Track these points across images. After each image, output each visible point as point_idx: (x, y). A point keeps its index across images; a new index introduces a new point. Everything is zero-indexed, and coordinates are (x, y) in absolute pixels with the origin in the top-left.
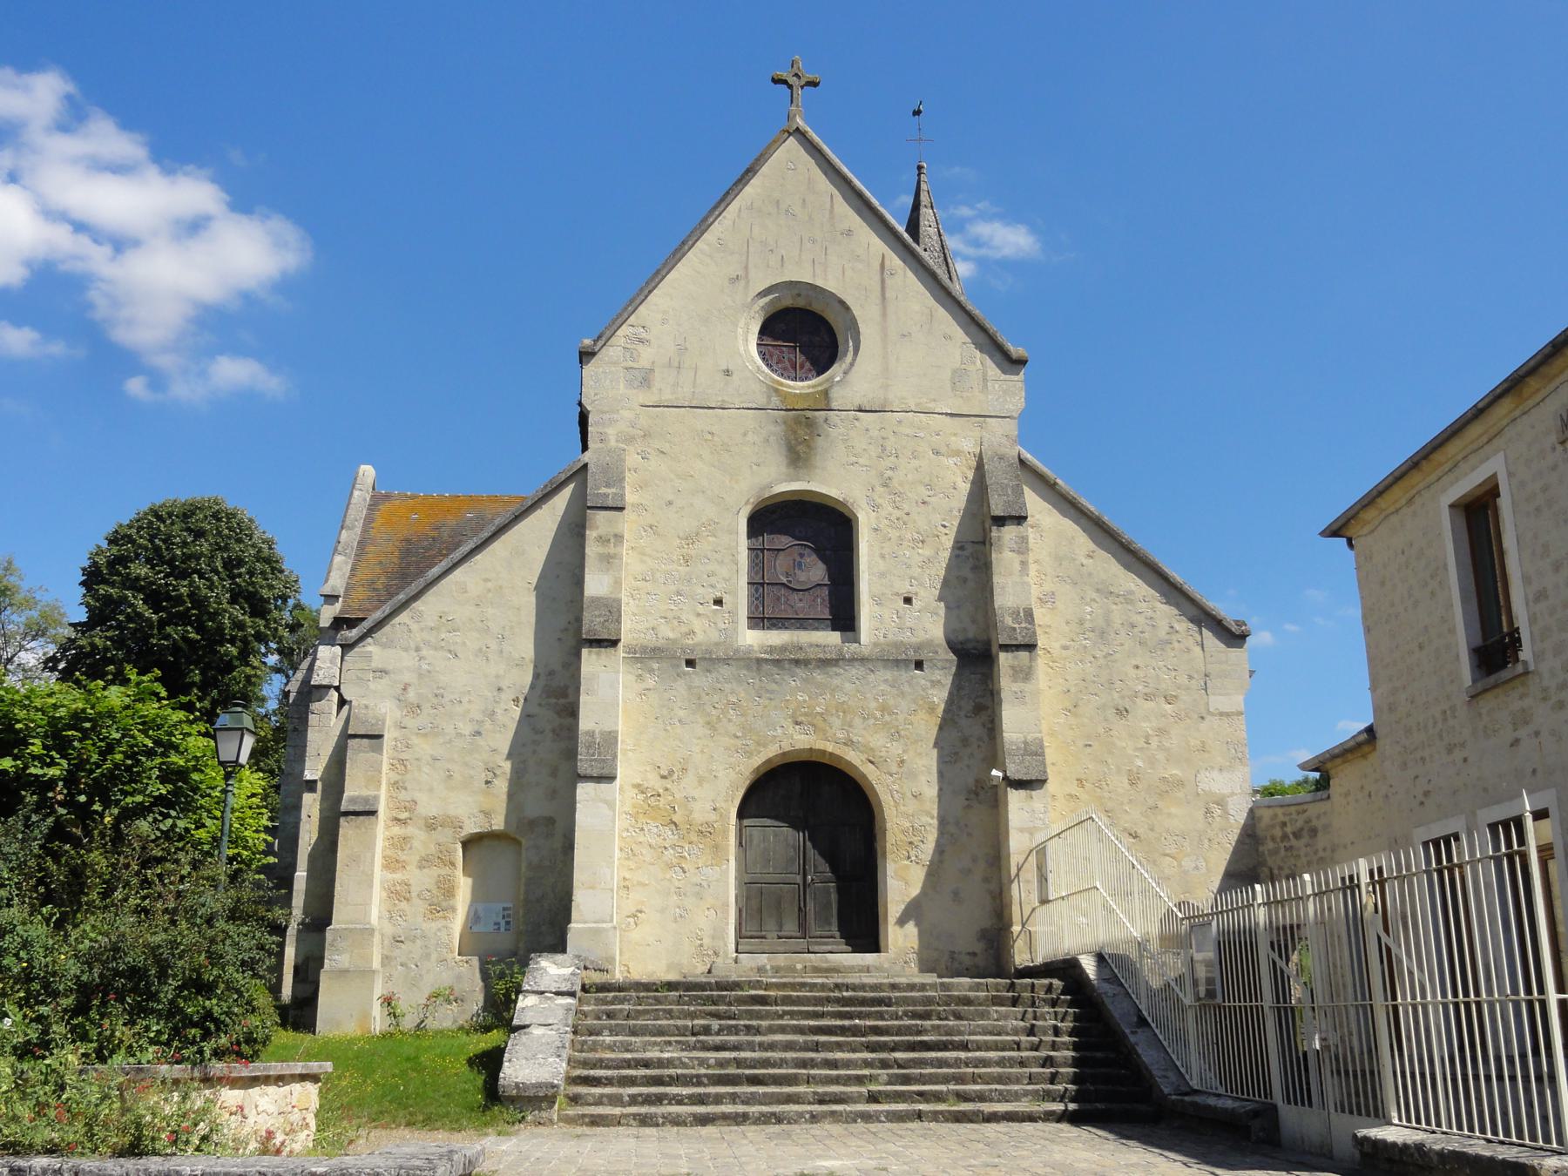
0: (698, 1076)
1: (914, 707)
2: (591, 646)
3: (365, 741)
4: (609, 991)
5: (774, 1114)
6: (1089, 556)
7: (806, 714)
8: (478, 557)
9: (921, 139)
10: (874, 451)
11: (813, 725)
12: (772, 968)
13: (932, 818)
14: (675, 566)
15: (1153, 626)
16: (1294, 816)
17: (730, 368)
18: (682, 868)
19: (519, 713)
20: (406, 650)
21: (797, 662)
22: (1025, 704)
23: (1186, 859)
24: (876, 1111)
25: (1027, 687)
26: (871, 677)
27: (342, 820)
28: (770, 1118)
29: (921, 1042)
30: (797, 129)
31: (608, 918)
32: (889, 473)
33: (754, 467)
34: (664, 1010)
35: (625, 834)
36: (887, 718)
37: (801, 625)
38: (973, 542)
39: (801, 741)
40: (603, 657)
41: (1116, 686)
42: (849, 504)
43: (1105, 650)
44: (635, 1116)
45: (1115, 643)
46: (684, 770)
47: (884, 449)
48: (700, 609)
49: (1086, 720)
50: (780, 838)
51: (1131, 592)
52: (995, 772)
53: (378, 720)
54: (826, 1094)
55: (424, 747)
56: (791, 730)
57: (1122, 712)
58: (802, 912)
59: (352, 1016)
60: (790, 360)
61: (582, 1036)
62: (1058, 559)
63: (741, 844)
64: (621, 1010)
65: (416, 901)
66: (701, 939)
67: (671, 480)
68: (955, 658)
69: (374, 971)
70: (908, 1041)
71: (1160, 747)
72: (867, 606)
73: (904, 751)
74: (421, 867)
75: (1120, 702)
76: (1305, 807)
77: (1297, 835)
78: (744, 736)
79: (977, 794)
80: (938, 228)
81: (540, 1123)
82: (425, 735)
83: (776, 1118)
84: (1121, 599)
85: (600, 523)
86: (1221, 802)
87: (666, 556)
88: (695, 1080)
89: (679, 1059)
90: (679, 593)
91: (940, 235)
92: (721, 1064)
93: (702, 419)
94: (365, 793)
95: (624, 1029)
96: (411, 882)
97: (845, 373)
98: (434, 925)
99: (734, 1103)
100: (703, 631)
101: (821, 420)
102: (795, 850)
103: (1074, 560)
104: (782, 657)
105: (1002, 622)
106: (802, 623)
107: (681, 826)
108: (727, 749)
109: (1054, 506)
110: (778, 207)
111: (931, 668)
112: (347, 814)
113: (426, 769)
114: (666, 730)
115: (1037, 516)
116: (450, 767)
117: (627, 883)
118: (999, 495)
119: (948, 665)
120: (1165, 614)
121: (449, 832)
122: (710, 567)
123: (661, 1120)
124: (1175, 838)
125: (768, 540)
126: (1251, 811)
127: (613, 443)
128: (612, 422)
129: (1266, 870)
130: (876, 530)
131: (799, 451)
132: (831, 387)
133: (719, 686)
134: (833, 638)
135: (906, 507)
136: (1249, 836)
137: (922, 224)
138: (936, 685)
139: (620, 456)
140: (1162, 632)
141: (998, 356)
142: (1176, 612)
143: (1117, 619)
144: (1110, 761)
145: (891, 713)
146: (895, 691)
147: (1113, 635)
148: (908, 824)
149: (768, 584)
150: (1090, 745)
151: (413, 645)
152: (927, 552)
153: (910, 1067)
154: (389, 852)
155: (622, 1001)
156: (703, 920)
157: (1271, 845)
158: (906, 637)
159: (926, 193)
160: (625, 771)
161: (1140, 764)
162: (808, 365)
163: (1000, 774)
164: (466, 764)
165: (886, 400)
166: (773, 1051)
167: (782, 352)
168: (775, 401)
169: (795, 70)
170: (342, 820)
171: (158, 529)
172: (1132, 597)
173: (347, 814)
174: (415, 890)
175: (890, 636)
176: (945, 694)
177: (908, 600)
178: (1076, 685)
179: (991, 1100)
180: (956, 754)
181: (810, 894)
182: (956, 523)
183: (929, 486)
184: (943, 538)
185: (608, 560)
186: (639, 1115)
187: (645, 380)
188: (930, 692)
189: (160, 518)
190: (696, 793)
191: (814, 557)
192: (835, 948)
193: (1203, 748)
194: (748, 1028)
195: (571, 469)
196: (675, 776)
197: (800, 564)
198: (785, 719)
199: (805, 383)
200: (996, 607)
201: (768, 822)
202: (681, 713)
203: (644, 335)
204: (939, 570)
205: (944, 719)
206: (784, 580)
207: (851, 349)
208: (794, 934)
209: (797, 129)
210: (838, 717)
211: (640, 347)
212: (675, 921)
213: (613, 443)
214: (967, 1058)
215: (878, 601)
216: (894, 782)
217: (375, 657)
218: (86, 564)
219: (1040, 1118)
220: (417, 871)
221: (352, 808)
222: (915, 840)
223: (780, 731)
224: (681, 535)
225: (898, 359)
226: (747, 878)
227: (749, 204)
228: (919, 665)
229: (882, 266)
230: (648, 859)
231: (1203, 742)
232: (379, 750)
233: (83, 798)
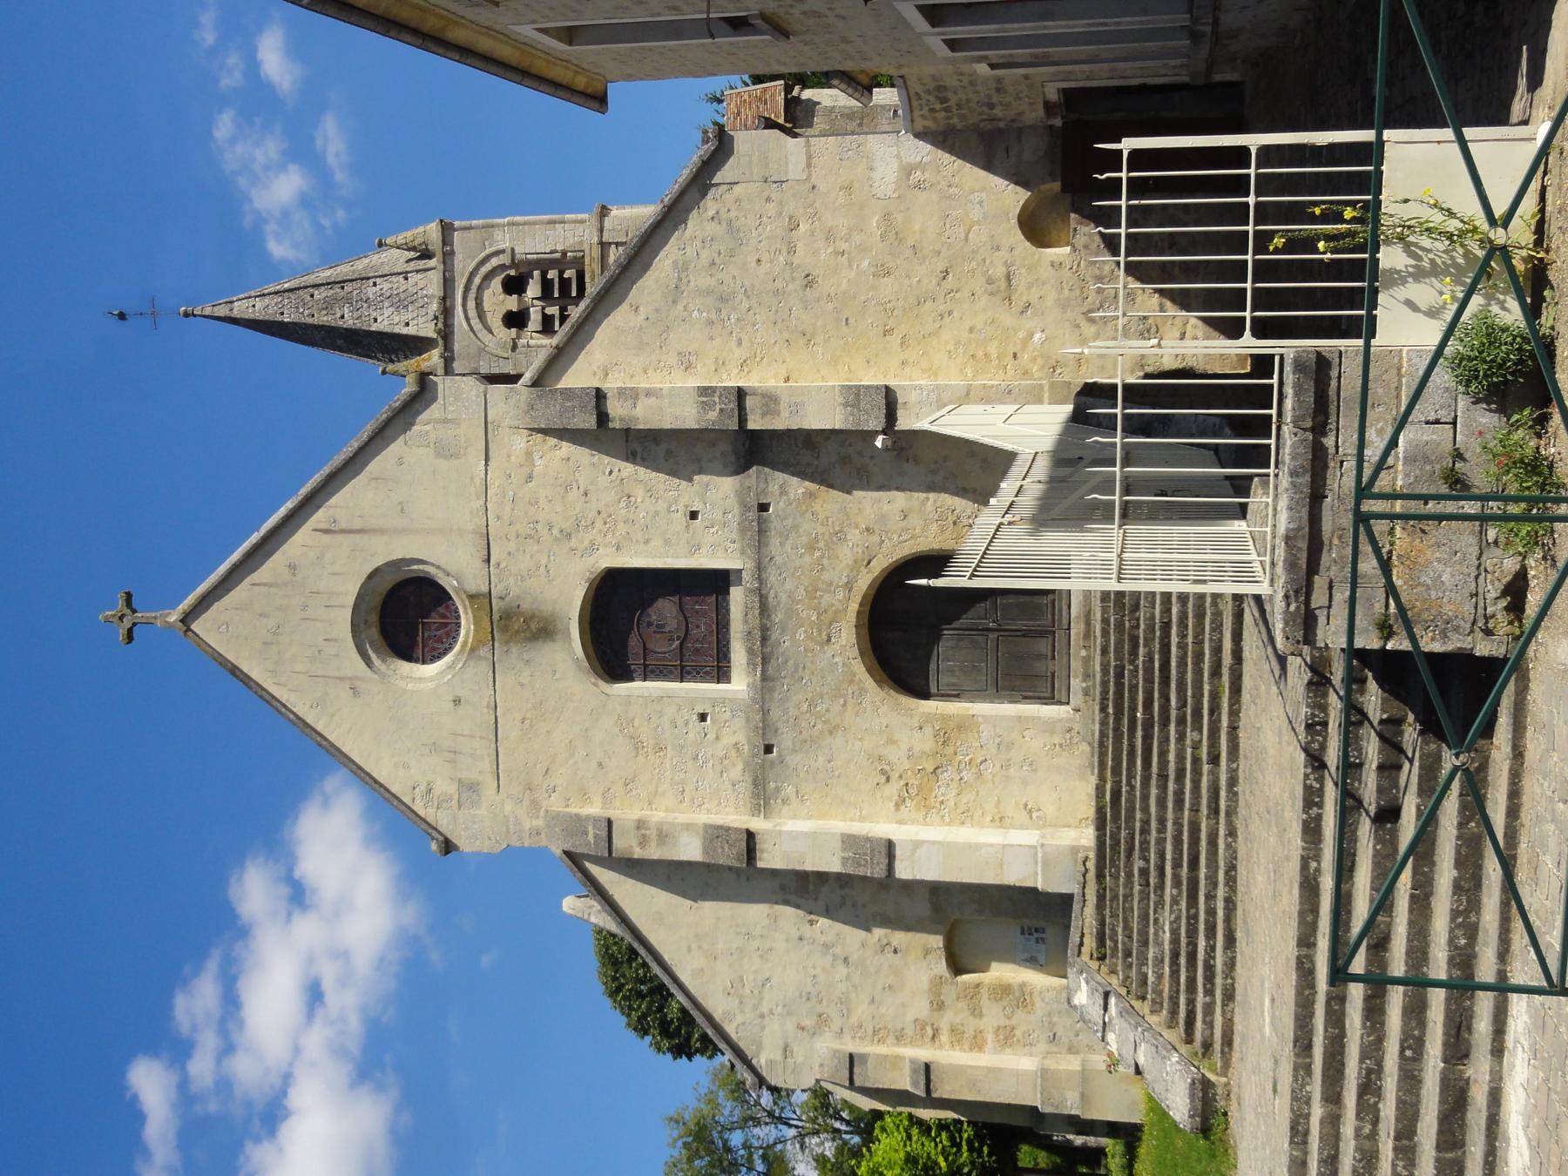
1: (808, 515)
2: (755, 858)
3: (856, 1070)
4: (1104, 934)
6: (636, 311)
7: (820, 631)
8: (666, 957)
9: (153, 313)
11: (831, 624)
12: (1084, 681)
13: (927, 499)
15: (712, 240)
16: (923, 102)
17: (451, 698)
18: (981, 763)
20: (763, 1028)
21: (764, 639)
23: (971, 216)
25: (785, 400)
26: (779, 560)
27: (934, 1095)
28: (1231, 876)
29: (1160, 670)
30: (182, 621)
31: (1032, 850)
32: (555, 531)
33: (557, 676)
34: (1124, 902)
36: (821, 544)
38: (627, 441)
39: (846, 636)
40: (765, 846)
41: (780, 286)
43: (741, 296)
44: (1224, 1005)
45: (732, 285)
47: (529, 537)
49: (820, 323)
51: (675, 263)
54: (1209, 807)
55: (861, 1011)
56: (836, 647)
57: (809, 281)
59: (1126, 1090)
60: (437, 630)
61: (1147, 993)
63: (957, 696)
65: (1014, 1021)
66: (1055, 745)
68: (754, 468)
69: (1083, 1070)
70: (1159, 684)
72: (702, 560)
74: (981, 1016)
75: (798, 282)
76: (912, 93)
77: (944, 100)
79: (902, 449)
80: (256, 297)
81: (1228, 1095)
83: (1230, 871)
84: (683, 276)
85: (625, 843)
86: (908, 170)
87: (657, 771)
88: (1192, 921)
89: (1171, 923)
90: (696, 758)
91: (264, 295)
92: (1177, 883)
94: (907, 1071)
95: (1142, 952)
96: (995, 1025)
97: (448, 575)
98: (1039, 1004)
99: (1215, 896)
100: (735, 734)
102: (963, 639)
103: (641, 329)
104: (759, 653)
108: (857, 715)
110: (271, 643)
111: (766, 495)
112: (928, 1090)
113: (883, 1010)
114: (839, 776)
116: (880, 987)
117: (997, 818)
118: (574, 416)
120: (698, 225)
121: (945, 989)
123: (1229, 981)
124: (948, 226)
125: (634, 662)
126: (917, 135)
127: (540, 823)
129: (982, 124)
130: (618, 548)
131: (539, 630)
134: (737, 595)
135: (592, 514)
136: (945, 141)
137: (251, 316)
141: (417, 406)
142: (695, 212)
143: (706, 281)
144: (863, 298)
145: (816, 540)
146: (793, 535)
148: (935, 525)
150: (847, 320)
151: (758, 1021)
152: (639, 494)
153: (1186, 695)
155: (1114, 933)
156: (1035, 743)
157: (955, 121)
158: (734, 517)
159: (216, 309)
160: (882, 829)
161: (866, 263)
162: (441, 610)
163: (881, 437)
164: (878, 972)
168: (484, 651)
169: (116, 620)
170: (934, 1095)
171: (630, 990)
173: (928, 1090)
174: (1003, 1022)
175: (734, 536)
176: (795, 480)
177: (694, 515)
178: (781, 332)
179: (1220, 640)
180: (859, 470)
182: (606, 459)
183: (567, 488)
184: (624, 474)
185: (663, 836)
186: (1223, 1001)
187: (470, 788)
189: (619, 989)
190: (904, 746)
191: (650, 611)
193: (848, 188)
196: (887, 768)
197: (659, 626)
198: (825, 653)
199: (463, 621)
200: (697, 427)
201: (933, 666)
202: (821, 760)
203: (423, 788)
204: (659, 479)
205: (821, 483)
209: (182, 621)
211: (436, 792)
213: (540, 823)
215: (695, 548)
217: (772, 1057)
218: (669, 1056)
219: (1240, 605)
220: (985, 1019)
222: (951, 519)
223: (837, 659)
224: (634, 754)
225: (429, 518)
227: (269, 674)
228: (763, 508)
229: (326, 531)
230: (972, 797)
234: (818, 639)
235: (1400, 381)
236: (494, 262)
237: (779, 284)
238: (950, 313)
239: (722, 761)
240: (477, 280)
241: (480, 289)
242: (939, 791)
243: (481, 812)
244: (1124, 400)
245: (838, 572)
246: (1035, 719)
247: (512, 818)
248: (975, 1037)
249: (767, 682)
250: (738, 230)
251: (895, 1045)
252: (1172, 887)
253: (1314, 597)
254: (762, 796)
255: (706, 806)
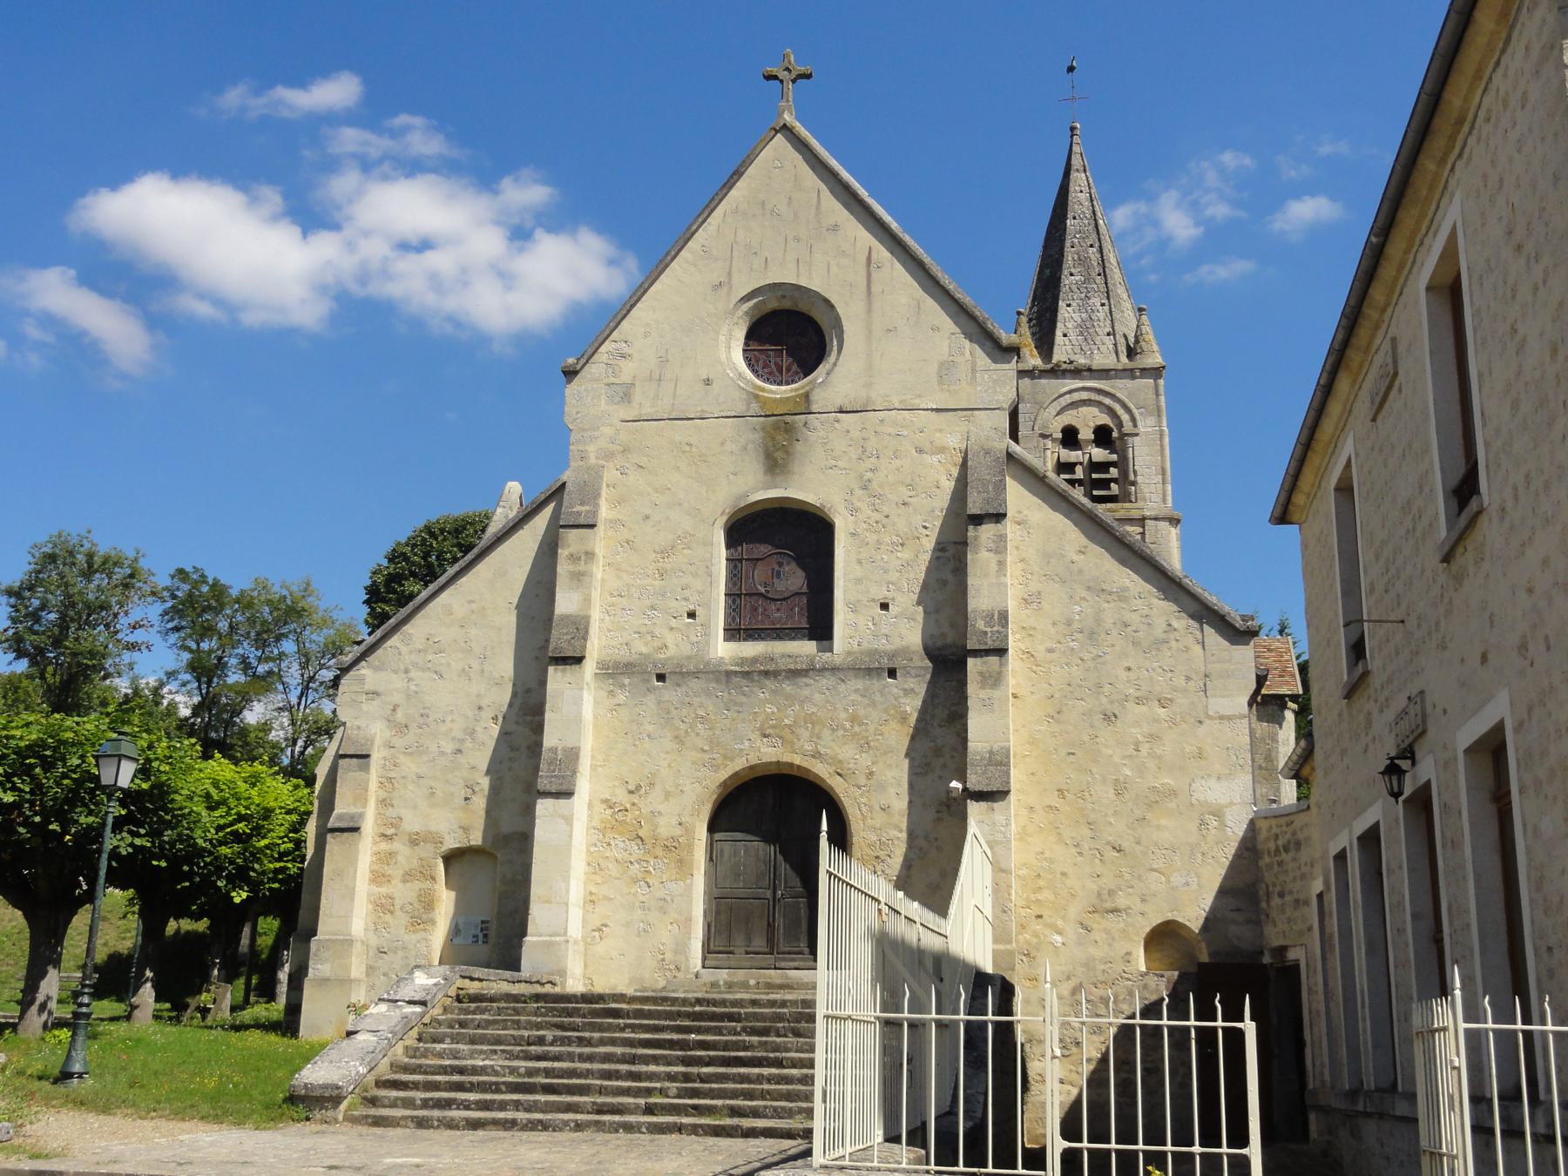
0: (497, 1084)
1: (885, 717)
2: (557, 664)
3: (355, 760)
5: (540, 1121)
7: (773, 727)
9: (1074, 98)
10: (854, 453)
11: (781, 738)
12: (726, 983)
13: (901, 831)
14: (650, 581)
15: (1149, 624)
16: (1284, 828)
18: (646, 882)
19: (498, 731)
20: (395, 672)
21: (766, 674)
22: (993, 711)
23: (1175, 874)
24: (638, 1123)
25: (996, 694)
26: (842, 687)
27: (329, 836)
28: (537, 1125)
30: (785, 125)
32: (869, 475)
33: (731, 477)
34: (512, 1021)
35: (593, 849)
36: (857, 729)
37: (778, 635)
38: (955, 543)
39: (768, 753)
40: (568, 675)
42: (826, 510)
45: (1105, 644)
46: (652, 784)
48: (674, 623)
50: (751, 851)
51: (1126, 589)
52: (954, 784)
53: (367, 740)
54: (604, 1104)
55: (410, 766)
56: (759, 743)
57: (1110, 717)
58: (771, 927)
62: (1047, 557)
63: (711, 859)
64: (473, 1020)
65: (398, 913)
66: (663, 954)
67: (649, 494)
71: (1152, 755)
73: (873, 764)
74: (404, 881)
75: (1109, 707)
76: (1291, 818)
77: (1286, 849)
78: (712, 749)
79: (948, 807)
80: (1090, 193)
82: (411, 754)
85: (572, 541)
86: (1218, 813)
87: (642, 571)
88: (494, 1087)
89: (492, 1066)
90: (653, 608)
91: (1092, 201)
92: (531, 1073)
93: (681, 432)
94: (353, 810)
98: (414, 937)
99: (518, 1110)
100: (675, 645)
101: (801, 424)
104: (753, 669)
105: (974, 626)
106: (779, 634)
107: (647, 841)
108: (694, 763)
109: (1043, 500)
112: (333, 830)
113: (411, 787)
114: (634, 745)
115: (1025, 513)
116: (433, 785)
117: (593, 897)
119: (923, 672)
120: (1163, 611)
121: (430, 847)
122: (686, 580)
123: (436, 1123)
124: (1164, 852)
125: (745, 550)
126: (1252, 822)
127: (593, 460)
128: (593, 439)
129: (1264, 886)
130: (853, 534)
131: (776, 459)
132: (812, 389)
133: (688, 700)
135: (885, 509)
136: (1247, 849)
138: (909, 696)
139: (597, 473)
140: (1159, 629)
141: (988, 344)
142: (1175, 608)
143: (1109, 619)
146: (866, 701)
147: (1103, 636)
149: (745, 595)
150: (1073, 754)
151: (402, 667)
152: (905, 555)
154: (375, 867)
155: (483, 1011)
156: (665, 935)
157: (1267, 860)
158: (882, 645)
160: (584, 786)
162: (795, 367)
163: (960, 786)
164: (447, 781)
165: (868, 399)
166: (591, 1062)
167: (768, 356)
168: (755, 408)
170: (329, 836)
171: (431, 545)
172: (1126, 594)
173: (333, 830)
174: (398, 903)
175: (865, 645)
176: (918, 703)
177: (884, 606)
179: (765, 1117)
180: (928, 764)
181: (780, 908)
182: (938, 524)
184: (924, 541)
185: (579, 577)
186: (417, 1117)
187: (625, 394)
188: (902, 701)
189: (432, 535)
190: (661, 808)
191: (793, 565)
192: (802, 964)
194: (580, 1039)
195: (551, 488)
201: (739, 835)
202: (650, 728)
203: (627, 351)
205: (916, 729)
206: (763, 590)
207: (835, 348)
208: (761, 950)
209: (785, 125)
210: (807, 729)
211: (622, 363)
212: (639, 935)
213: (593, 460)
214: (770, 1075)
215: (853, 608)
216: (862, 795)
217: (368, 680)
218: (369, 583)
219: (799, 1135)
220: (401, 885)
221: (337, 825)
222: (882, 854)
223: (747, 743)
224: (657, 548)
226: (717, 893)
227: (734, 206)
228: (892, 673)
230: (614, 873)
231: (1199, 748)
232: (366, 769)
233: (37, 819)
234: (766, 725)
236: (1125, 417)
240: (1107, 401)
241: (1099, 404)
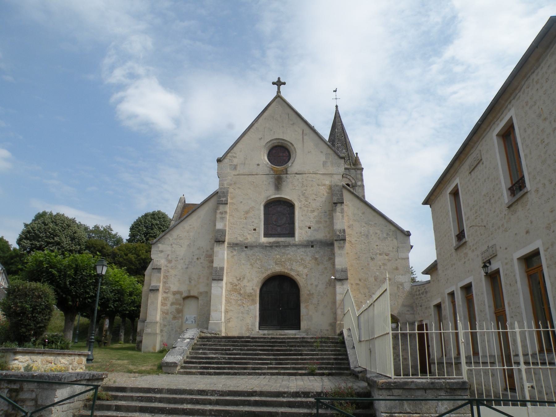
7: (279, 261)
21: (277, 246)
26: (298, 250)
32: (305, 191)
33: (266, 191)
36: (303, 262)
39: (278, 269)
47: (303, 185)
55: (172, 272)
57: (372, 259)
69: (157, 334)
76: (424, 285)
90: (243, 228)
92: (229, 358)
97: (292, 163)
100: (250, 239)
108: (256, 272)
113: (173, 278)
135: (309, 201)
144: (369, 273)
151: (170, 244)
156: (249, 321)
160: (225, 278)
161: (378, 274)
168: (272, 172)
180: (323, 272)
183: (316, 195)
185: (223, 219)
190: (247, 285)
203: (235, 155)
213: (226, 186)
215: (301, 228)
217: (160, 247)
235: (462, 414)
237: (371, 251)
238: (365, 296)
239: (243, 235)
242: (235, 294)
243: (229, 170)
244: (436, 332)
245: (295, 266)
246: (255, 320)
247: (226, 178)
248: (165, 304)
249: (264, 247)
250: (385, 240)
251: (163, 281)
252: (228, 357)
253: (396, 390)
254: (233, 246)
255: (230, 230)
